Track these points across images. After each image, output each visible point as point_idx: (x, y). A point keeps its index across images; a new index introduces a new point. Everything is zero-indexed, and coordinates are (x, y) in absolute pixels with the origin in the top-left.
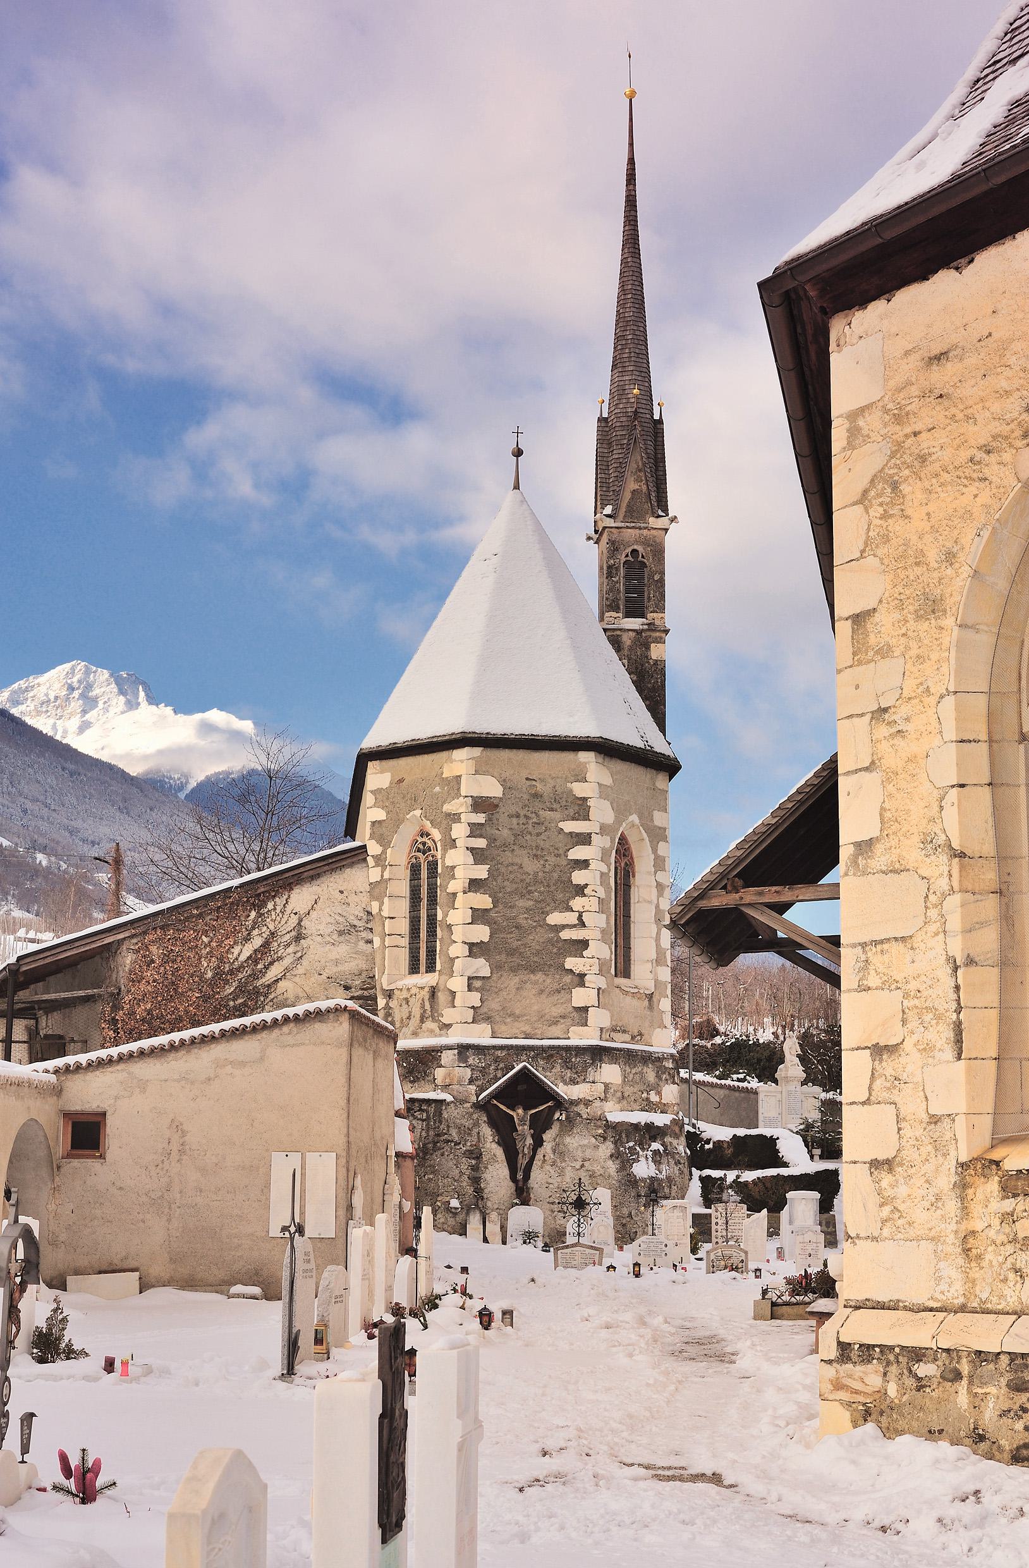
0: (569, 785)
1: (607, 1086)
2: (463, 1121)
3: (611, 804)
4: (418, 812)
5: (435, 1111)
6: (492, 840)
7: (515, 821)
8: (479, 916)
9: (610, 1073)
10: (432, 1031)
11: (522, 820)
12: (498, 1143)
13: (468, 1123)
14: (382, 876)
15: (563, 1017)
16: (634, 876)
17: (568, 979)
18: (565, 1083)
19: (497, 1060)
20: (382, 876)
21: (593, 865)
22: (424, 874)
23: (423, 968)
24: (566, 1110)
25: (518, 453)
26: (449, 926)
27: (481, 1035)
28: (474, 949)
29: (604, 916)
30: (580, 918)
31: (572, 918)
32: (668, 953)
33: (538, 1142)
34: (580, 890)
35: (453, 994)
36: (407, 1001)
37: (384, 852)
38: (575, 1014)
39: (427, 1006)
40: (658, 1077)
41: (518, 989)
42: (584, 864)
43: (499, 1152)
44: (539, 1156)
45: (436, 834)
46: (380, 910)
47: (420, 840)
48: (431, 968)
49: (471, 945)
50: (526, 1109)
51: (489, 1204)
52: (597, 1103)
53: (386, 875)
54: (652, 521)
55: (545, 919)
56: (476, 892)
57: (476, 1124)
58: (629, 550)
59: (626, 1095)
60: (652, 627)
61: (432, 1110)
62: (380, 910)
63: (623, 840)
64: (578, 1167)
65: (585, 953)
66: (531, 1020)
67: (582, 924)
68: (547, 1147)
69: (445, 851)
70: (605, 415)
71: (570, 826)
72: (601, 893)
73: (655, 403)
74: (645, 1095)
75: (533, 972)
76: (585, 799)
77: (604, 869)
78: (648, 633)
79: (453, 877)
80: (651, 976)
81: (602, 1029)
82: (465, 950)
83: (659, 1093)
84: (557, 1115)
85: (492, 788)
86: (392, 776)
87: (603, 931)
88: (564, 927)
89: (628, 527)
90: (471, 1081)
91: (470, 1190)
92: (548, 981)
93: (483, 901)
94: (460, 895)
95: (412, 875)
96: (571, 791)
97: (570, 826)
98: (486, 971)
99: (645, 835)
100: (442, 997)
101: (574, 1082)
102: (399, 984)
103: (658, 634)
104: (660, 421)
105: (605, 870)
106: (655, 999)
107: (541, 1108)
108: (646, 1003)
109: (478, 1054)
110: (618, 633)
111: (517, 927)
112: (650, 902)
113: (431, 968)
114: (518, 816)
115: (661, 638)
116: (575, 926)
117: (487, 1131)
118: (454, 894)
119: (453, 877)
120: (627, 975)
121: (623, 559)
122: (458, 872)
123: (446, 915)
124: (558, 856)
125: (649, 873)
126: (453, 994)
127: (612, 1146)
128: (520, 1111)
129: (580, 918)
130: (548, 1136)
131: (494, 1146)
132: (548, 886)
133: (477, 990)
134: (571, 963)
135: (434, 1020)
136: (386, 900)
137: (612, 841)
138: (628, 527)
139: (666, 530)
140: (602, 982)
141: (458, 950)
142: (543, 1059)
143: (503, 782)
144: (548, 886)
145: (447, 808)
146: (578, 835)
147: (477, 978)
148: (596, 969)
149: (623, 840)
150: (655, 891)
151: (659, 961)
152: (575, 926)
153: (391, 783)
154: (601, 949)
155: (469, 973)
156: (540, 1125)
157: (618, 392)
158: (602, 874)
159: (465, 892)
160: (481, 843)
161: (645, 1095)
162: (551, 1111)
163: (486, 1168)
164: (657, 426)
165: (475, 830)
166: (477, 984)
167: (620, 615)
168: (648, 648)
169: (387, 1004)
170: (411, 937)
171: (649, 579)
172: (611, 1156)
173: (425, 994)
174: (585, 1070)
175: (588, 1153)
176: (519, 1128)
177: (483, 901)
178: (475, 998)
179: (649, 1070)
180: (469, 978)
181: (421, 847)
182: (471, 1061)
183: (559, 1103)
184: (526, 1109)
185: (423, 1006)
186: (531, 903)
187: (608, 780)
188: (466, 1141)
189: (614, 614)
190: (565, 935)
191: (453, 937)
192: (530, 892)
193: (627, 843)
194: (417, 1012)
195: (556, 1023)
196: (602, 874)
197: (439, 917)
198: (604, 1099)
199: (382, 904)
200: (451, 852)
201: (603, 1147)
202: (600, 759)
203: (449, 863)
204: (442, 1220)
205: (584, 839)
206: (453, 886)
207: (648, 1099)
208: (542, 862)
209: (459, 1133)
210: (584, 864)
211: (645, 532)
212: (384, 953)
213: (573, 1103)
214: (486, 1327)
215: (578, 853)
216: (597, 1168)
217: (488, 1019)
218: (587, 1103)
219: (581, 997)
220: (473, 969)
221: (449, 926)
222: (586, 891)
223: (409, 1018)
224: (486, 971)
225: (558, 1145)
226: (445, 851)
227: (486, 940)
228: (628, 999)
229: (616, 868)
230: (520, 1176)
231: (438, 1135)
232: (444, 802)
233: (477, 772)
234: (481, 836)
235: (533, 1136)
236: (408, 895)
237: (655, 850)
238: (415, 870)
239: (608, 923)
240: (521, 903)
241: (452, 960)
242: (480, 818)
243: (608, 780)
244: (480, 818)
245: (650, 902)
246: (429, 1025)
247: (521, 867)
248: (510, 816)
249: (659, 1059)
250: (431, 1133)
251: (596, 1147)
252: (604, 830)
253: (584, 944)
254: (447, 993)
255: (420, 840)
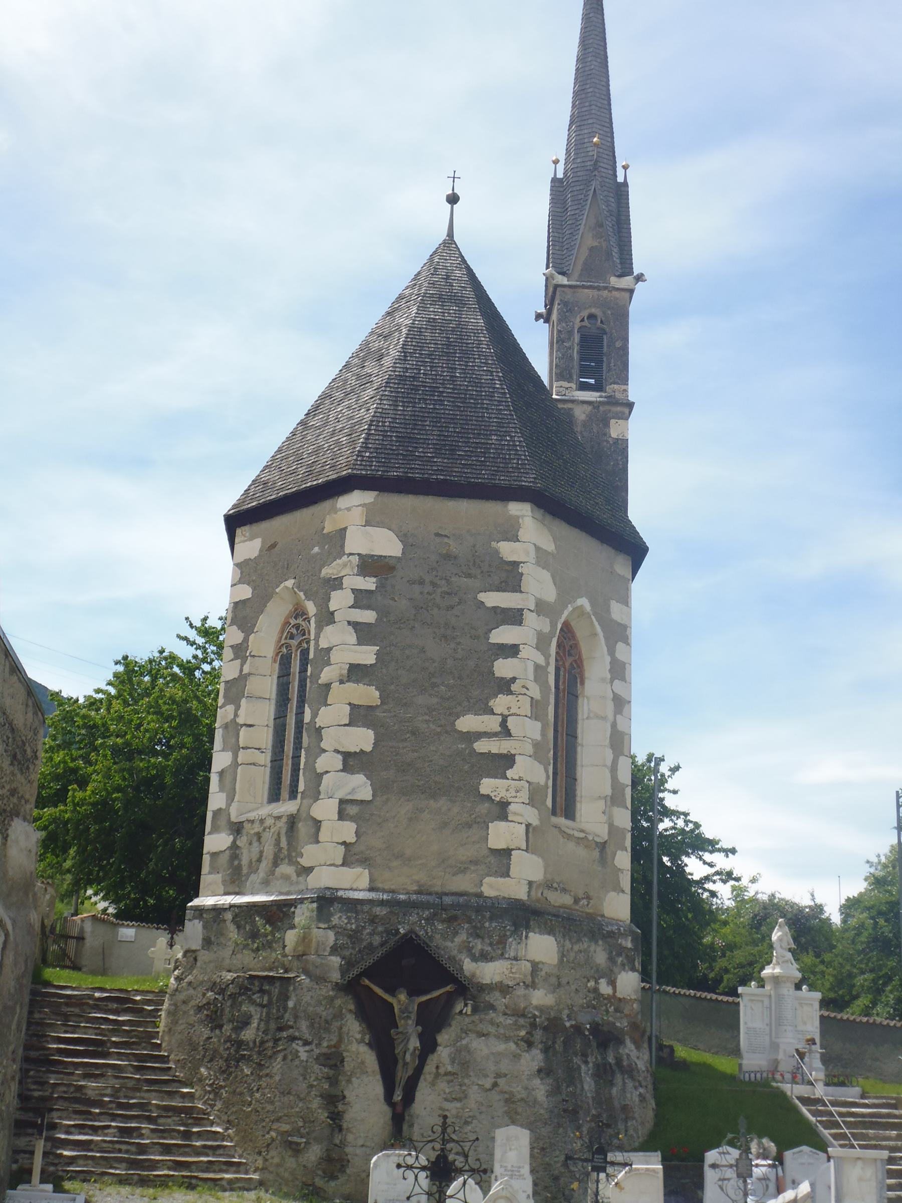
0: (494, 544)
1: (536, 967)
2: (320, 1009)
3: (553, 577)
4: (290, 583)
5: (280, 993)
6: (383, 613)
7: (417, 588)
8: (359, 715)
9: (541, 947)
10: (286, 878)
11: (428, 588)
12: (370, 1045)
13: (325, 1013)
14: (241, 670)
15: (475, 862)
16: (582, 683)
17: (483, 808)
18: (474, 959)
19: (373, 920)
20: (241, 670)
21: (525, 652)
22: (296, 667)
23: (285, 794)
24: (473, 998)
25: (453, 199)
26: (319, 730)
27: (354, 882)
28: (352, 761)
29: (538, 725)
30: (504, 723)
31: (491, 723)
32: (628, 791)
33: (429, 1046)
34: (505, 686)
35: (317, 824)
36: (259, 836)
37: (246, 640)
38: (492, 859)
39: (284, 843)
40: (611, 959)
41: (410, 819)
42: (512, 650)
43: (370, 1059)
44: (429, 1068)
45: (311, 608)
46: (236, 715)
47: (293, 622)
48: (293, 794)
49: (347, 756)
50: (413, 993)
51: (350, 1138)
52: (521, 991)
53: (246, 670)
54: (614, 281)
55: (453, 724)
56: (357, 682)
57: (339, 1016)
58: (585, 314)
59: (564, 981)
60: (612, 401)
61: (276, 991)
62: (236, 715)
63: (567, 631)
64: (488, 1086)
65: (509, 773)
66: (428, 860)
67: (505, 732)
68: (443, 1053)
69: (319, 629)
70: (560, 175)
71: (492, 599)
72: (535, 691)
73: (620, 164)
74: (591, 984)
75: (433, 796)
76: (516, 564)
77: (541, 660)
78: (607, 407)
79: (328, 663)
80: (604, 818)
81: (530, 883)
82: (337, 762)
83: (612, 983)
84: (459, 1006)
85: (386, 544)
86: (263, 542)
87: (536, 745)
88: (479, 735)
89: (584, 287)
90: (334, 950)
91: (323, 1115)
92: (456, 810)
93: (368, 694)
94: (335, 685)
95: (281, 669)
96: (497, 552)
97: (492, 599)
98: (365, 792)
99: (599, 629)
100: (303, 828)
101: (485, 957)
102: (252, 816)
103: (619, 409)
104: (625, 184)
105: (541, 660)
106: (609, 851)
107: (436, 994)
108: (596, 854)
109: (347, 911)
110: (570, 406)
111: (413, 733)
112: (604, 718)
113: (293, 794)
114: (421, 582)
115: (623, 413)
116: (495, 735)
117: (353, 1027)
118: (328, 686)
119: (328, 663)
120: (569, 812)
121: (577, 324)
122: (334, 657)
123: (315, 715)
124: (477, 637)
125: (603, 680)
126: (317, 824)
127: (540, 1057)
128: (403, 997)
129: (504, 723)
130: (443, 1038)
131: (364, 1049)
132: (460, 678)
133: (352, 819)
134: (488, 785)
135: (292, 861)
136: (243, 701)
137: (553, 625)
138: (584, 287)
139: (631, 291)
140: (532, 816)
141: (328, 762)
142: (443, 921)
143: (403, 537)
144: (460, 678)
145: (326, 572)
146: (505, 611)
147: (352, 802)
148: (524, 796)
149: (567, 631)
150: (610, 706)
151: (615, 799)
152: (495, 735)
153: (261, 551)
154: (530, 770)
155: (341, 794)
156: (433, 1022)
157: (578, 145)
158: (537, 667)
159: (341, 682)
160: (368, 616)
161: (591, 984)
162: (449, 1001)
163: (349, 1081)
164: (621, 192)
165: (361, 599)
166: (352, 810)
167: (574, 386)
168: (607, 425)
169: (234, 842)
170: (274, 753)
171: (609, 346)
172: (540, 1071)
173: (282, 824)
174: (503, 941)
175: (505, 1066)
176: (401, 1023)
177: (368, 694)
178: (348, 832)
179: (599, 949)
180: (342, 802)
181: (294, 631)
182: (335, 920)
183: (464, 989)
184: (411, 994)
185: (278, 842)
186: (435, 700)
187: (549, 546)
188: (321, 1039)
189: (565, 384)
190: (482, 746)
191: (323, 745)
192: (434, 685)
193: (574, 637)
194: (269, 850)
195: (463, 871)
196: (537, 667)
197: (307, 718)
198: (533, 985)
199: (238, 708)
200: (329, 629)
201: (526, 1056)
202: (539, 513)
203: (323, 644)
204: (276, 1160)
205: (514, 617)
206: (326, 674)
207: (596, 990)
208: (453, 645)
209: (312, 1026)
210: (512, 650)
211: (605, 293)
212: (235, 773)
213: (490, 988)
214: (808, 1040)
215: (503, 635)
216: (518, 1090)
217: (365, 861)
218: (504, 989)
219: (501, 835)
220: (348, 789)
221: (319, 730)
222: (514, 687)
223: (259, 860)
224: (365, 792)
225: (459, 1051)
226: (319, 629)
227: (368, 748)
228: (571, 845)
229: (557, 669)
230: (398, 1097)
231: (280, 1029)
232: (323, 566)
233: (368, 523)
234: (368, 607)
235: (421, 1036)
236: (274, 696)
237: (612, 652)
238: (285, 662)
239: (543, 733)
240: (421, 700)
241: (320, 776)
242: (369, 584)
243: (549, 546)
244: (369, 584)
245: (604, 718)
246: (285, 869)
247: (423, 650)
248: (412, 582)
249: (611, 935)
250: (273, 1026)
251: (516, 1057)
252: (541, 608)
253: (509, 760)
254: (310, 823)
255: (293, 622)
